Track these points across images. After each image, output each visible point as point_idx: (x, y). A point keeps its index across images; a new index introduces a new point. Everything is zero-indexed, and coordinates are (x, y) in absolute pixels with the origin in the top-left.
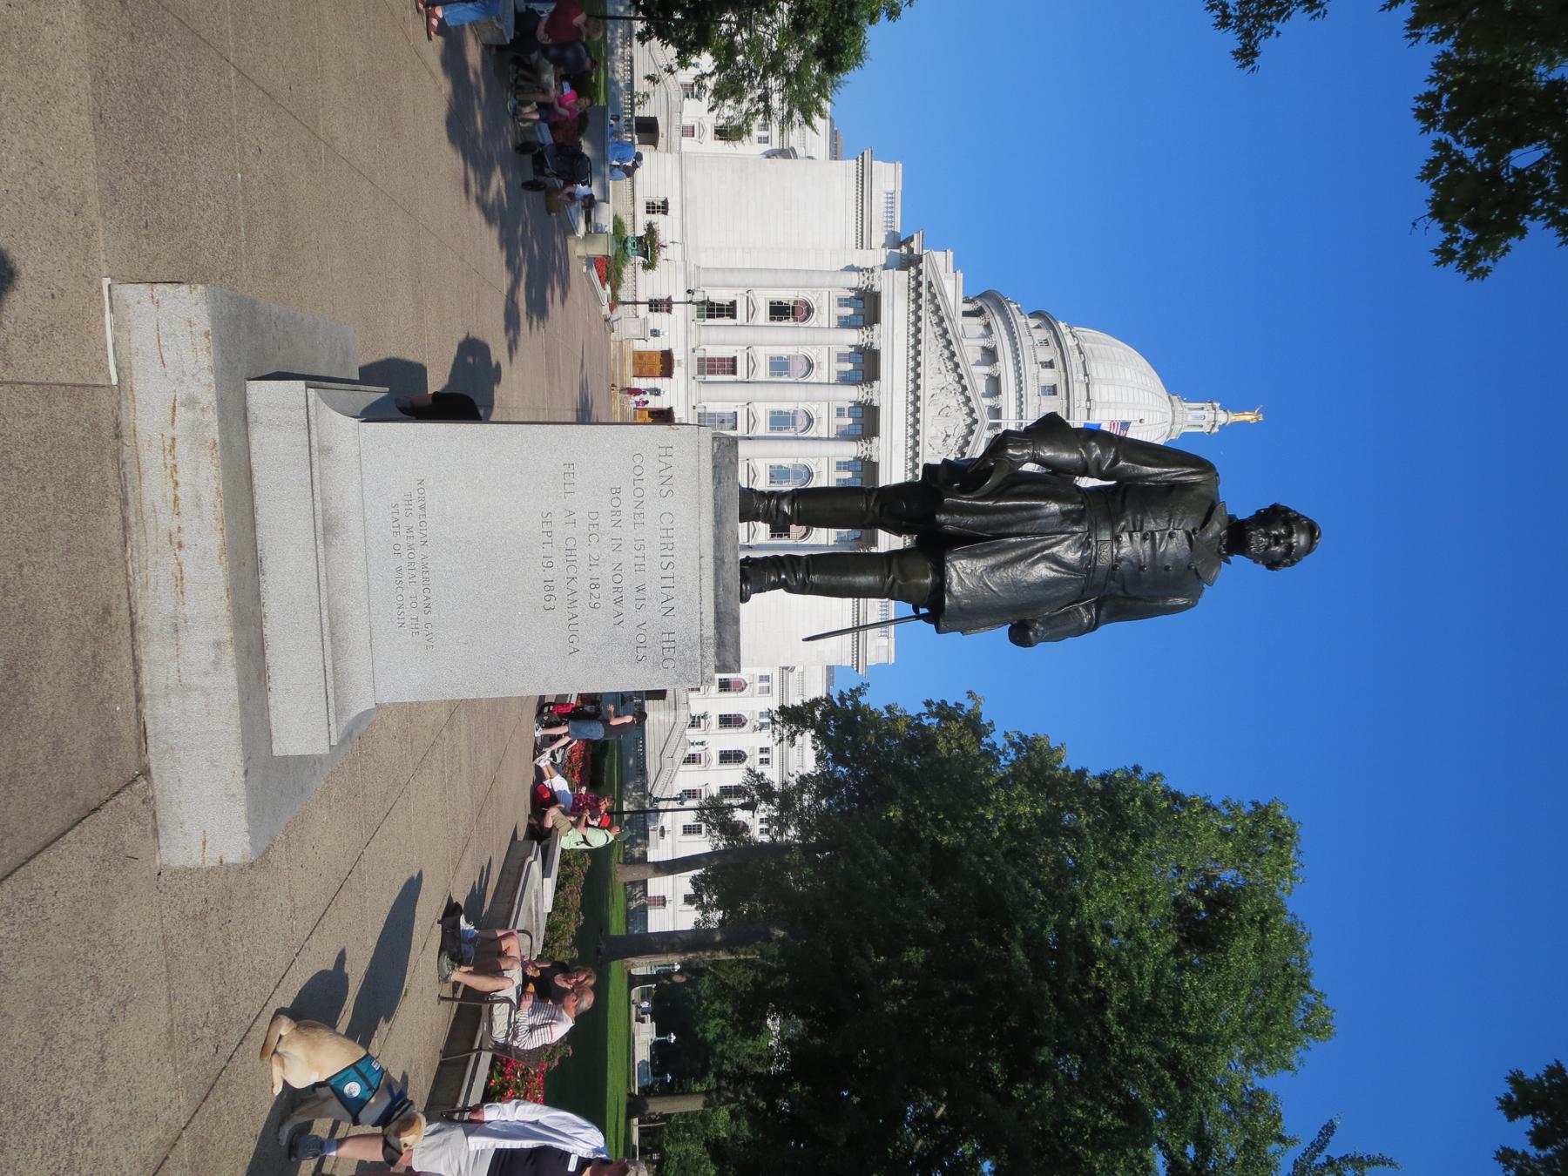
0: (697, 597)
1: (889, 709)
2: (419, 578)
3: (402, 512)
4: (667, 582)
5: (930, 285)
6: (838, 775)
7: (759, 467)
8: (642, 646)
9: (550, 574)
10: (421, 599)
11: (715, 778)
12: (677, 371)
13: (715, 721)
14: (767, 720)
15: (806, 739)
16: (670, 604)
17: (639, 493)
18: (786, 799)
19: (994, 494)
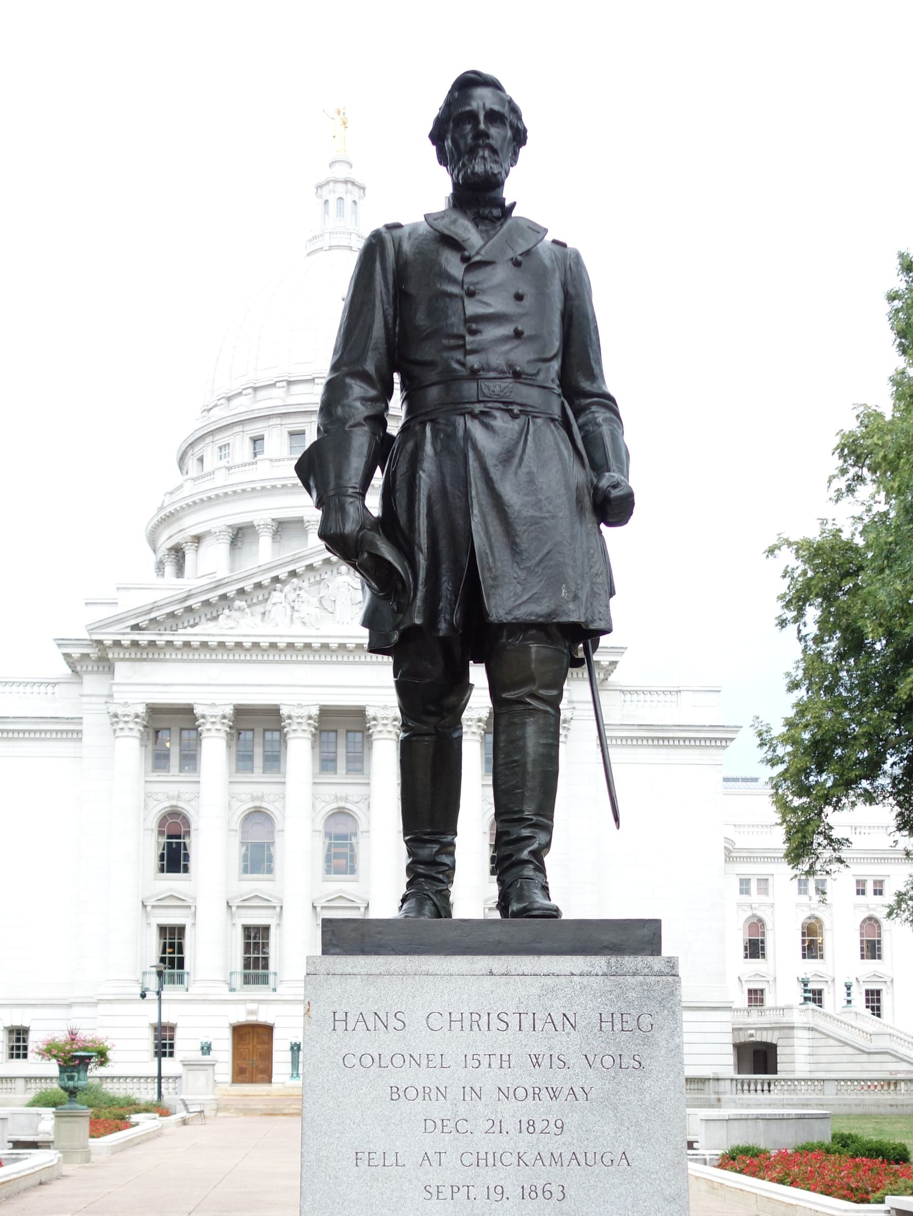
0: (549, 981)
1: (794, 686)
4: (527, 1022)
5: (136, 627)
6: (897, 771)
7: (381, 885)
9: (512, 1191)
12: (263, 1016)
13: (811, 967)
14: (812, 883)
15: (840, 820)
17: (398, 1060)
19: (407, 550)
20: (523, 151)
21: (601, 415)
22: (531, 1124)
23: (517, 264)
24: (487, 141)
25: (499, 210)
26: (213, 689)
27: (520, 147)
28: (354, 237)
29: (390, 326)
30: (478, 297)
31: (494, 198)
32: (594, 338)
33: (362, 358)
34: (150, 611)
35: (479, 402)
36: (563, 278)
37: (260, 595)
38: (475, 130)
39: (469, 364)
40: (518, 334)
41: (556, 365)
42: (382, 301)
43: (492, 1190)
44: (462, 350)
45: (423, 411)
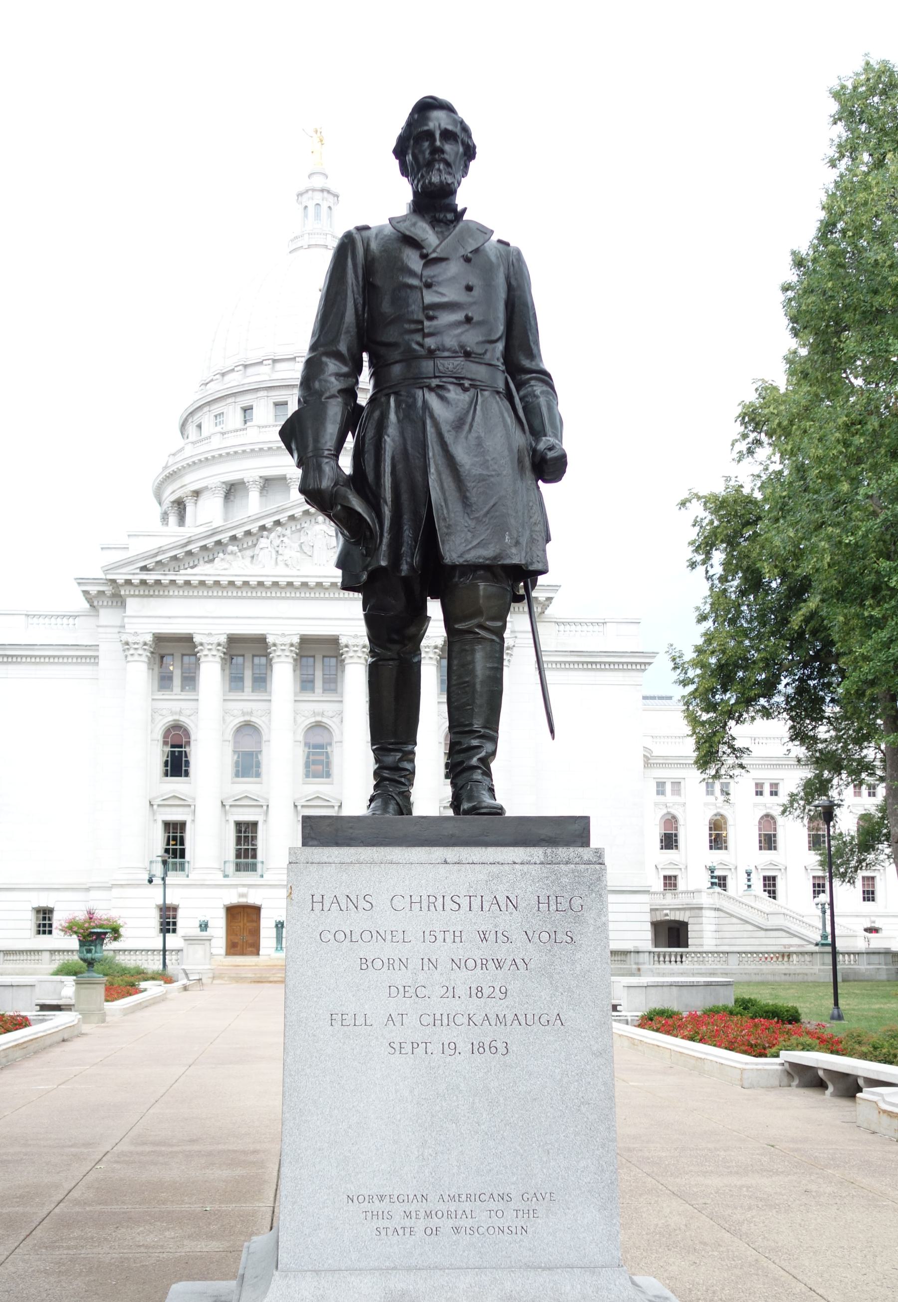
0: (495, 869)
1: (703, 618)
2: (467, 1206)
3: (386, 1223)
4: (476, 903)
5: (144, 569)
6: (790, 690)
7: (352, 788)
8: (553, 936)
9: (464, 1047)
10: (492, 1205)
11: (796, 856)
12: (252, 899)
14: (717, 785)
16: (502, 900)
17: (366, 936)
18: (829, 762)
19: (375, 505)
20: (472, 164)
22: (480, 990)
23: (467, 260)
26: (209, 621)
27: (470, 161)
29: (360, 313)
30: (434, 288)
32: (533, 323)
34: (156, 555)
35: (435, 377)
37: (250, 541)
38: (432, 146)
39: (427, 345)
40: (468, 320)
41: (500, 346)
42: (353, 292)
43: (446, 1046)
45: (388, 385)
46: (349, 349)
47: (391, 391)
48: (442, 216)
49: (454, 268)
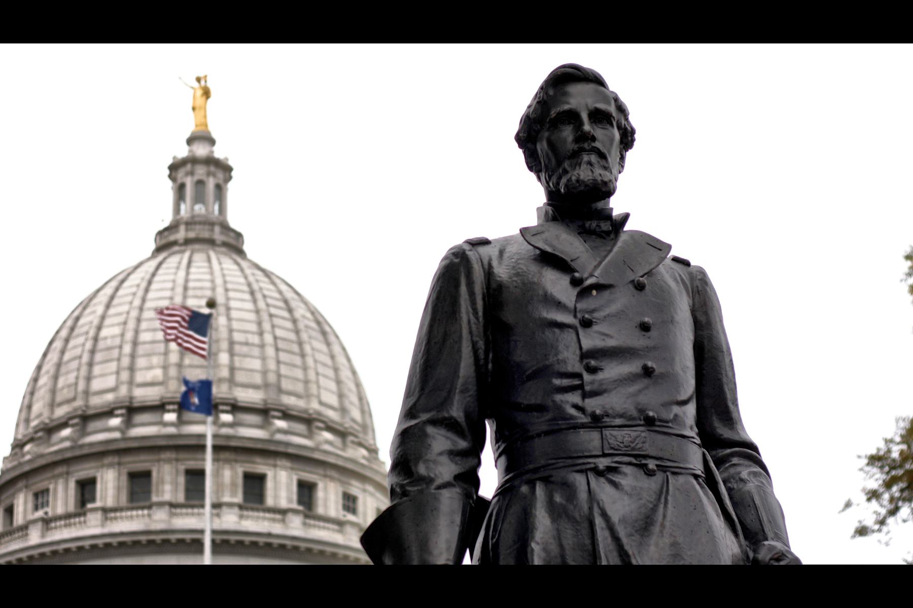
20: (629, 155)
21: (746, 471)
23: (639, 287)
24: (593, 144)
25: (609, 223)
27: (627, 150)
28: (217, 229)
29: (482, 362)
30: (595, 328)
31: (603, 209)
32: (730, 374)
33: (446, 402)
35: (604, 455)
36: (691, 302)
39: (589, 410)
40: (647, 372)
41: (691, 410)
42: (471, 332)
44: (580, 392)
45: (531, 466)
46: (467, 415)
47: (537, 476)
48: (594, 224)
49: (621, 300)
